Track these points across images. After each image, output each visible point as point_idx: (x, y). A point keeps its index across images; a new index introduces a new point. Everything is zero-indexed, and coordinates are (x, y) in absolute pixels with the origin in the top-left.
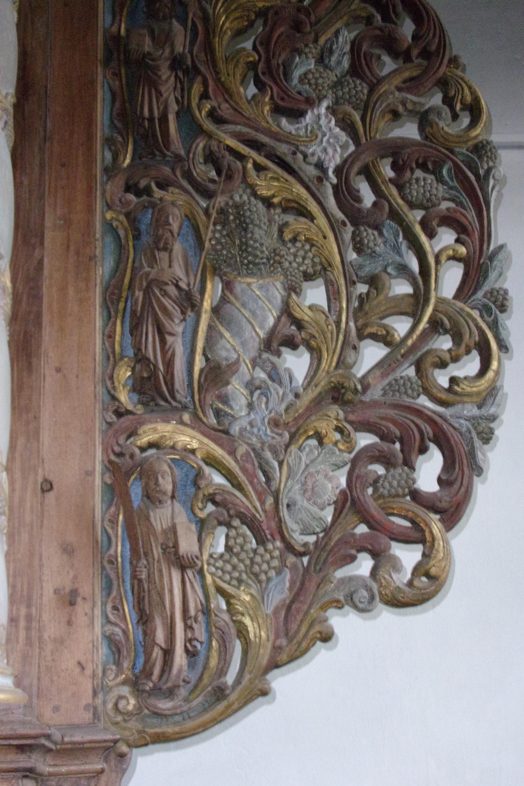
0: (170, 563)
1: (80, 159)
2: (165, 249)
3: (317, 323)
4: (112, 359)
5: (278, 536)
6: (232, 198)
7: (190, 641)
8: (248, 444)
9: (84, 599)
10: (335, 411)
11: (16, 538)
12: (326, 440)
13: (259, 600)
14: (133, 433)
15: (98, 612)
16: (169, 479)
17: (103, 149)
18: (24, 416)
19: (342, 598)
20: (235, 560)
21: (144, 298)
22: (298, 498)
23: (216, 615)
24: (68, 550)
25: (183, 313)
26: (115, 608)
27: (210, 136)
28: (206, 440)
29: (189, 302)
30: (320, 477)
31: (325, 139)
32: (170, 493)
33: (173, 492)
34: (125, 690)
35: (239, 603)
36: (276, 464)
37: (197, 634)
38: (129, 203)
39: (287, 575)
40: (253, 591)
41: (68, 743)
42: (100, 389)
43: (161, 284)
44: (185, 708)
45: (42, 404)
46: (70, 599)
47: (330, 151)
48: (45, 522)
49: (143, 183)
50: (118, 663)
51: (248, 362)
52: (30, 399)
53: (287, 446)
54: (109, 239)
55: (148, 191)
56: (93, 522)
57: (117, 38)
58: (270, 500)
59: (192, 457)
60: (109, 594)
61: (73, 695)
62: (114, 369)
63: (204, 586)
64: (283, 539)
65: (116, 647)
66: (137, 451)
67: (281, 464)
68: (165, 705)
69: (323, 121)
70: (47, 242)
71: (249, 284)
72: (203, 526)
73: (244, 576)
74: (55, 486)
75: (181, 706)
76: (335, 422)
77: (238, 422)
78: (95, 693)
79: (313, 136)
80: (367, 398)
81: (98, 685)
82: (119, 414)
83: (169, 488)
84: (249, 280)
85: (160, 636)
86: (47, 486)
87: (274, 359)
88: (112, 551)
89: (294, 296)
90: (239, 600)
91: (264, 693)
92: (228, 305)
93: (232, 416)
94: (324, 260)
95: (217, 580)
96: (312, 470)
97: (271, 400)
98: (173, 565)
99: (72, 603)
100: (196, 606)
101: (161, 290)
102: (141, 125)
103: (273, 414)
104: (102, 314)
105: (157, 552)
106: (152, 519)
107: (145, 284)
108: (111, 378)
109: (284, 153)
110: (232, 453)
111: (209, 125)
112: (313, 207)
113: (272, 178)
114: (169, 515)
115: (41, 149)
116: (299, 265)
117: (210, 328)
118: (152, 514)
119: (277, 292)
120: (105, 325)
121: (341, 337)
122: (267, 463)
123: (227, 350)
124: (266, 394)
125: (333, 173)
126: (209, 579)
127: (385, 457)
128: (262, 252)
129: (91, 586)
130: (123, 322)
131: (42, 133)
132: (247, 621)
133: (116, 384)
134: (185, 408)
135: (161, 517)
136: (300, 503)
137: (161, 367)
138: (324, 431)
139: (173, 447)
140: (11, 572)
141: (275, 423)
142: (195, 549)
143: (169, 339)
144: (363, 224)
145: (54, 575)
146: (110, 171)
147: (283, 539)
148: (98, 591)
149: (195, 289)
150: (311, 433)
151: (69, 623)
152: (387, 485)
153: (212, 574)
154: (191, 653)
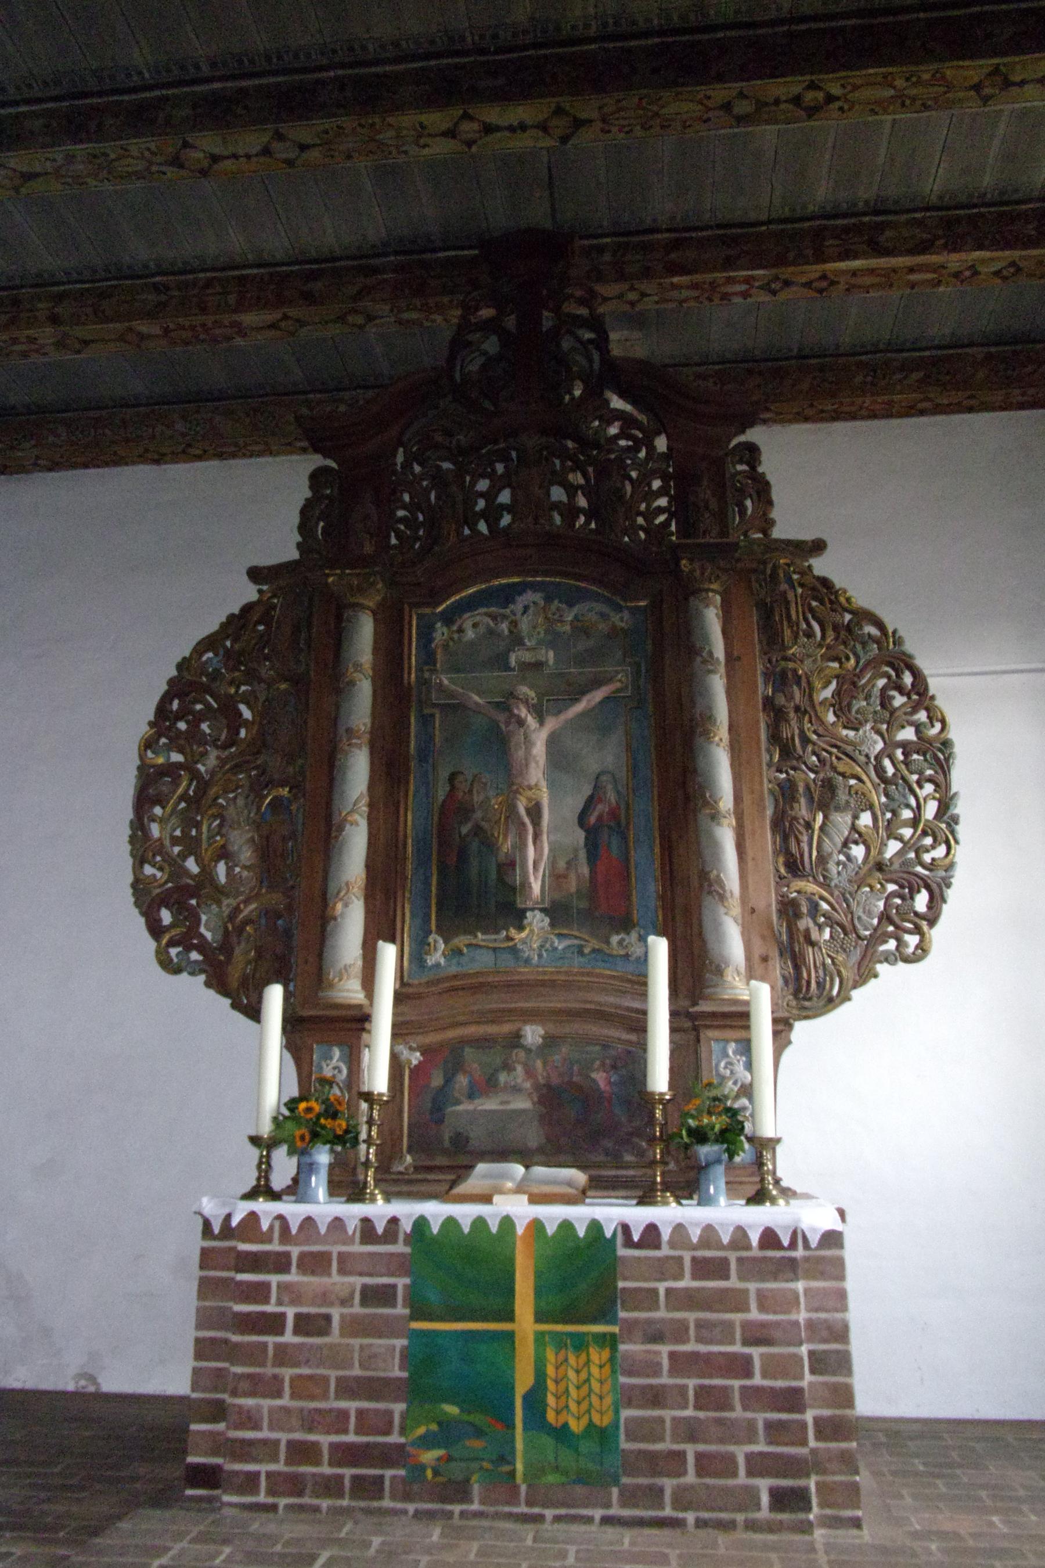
29: (809, 826)
46: (765, 959)
111: (814, 737)
119: (849, 819)
129: (774, 953)
145: (759, 950)
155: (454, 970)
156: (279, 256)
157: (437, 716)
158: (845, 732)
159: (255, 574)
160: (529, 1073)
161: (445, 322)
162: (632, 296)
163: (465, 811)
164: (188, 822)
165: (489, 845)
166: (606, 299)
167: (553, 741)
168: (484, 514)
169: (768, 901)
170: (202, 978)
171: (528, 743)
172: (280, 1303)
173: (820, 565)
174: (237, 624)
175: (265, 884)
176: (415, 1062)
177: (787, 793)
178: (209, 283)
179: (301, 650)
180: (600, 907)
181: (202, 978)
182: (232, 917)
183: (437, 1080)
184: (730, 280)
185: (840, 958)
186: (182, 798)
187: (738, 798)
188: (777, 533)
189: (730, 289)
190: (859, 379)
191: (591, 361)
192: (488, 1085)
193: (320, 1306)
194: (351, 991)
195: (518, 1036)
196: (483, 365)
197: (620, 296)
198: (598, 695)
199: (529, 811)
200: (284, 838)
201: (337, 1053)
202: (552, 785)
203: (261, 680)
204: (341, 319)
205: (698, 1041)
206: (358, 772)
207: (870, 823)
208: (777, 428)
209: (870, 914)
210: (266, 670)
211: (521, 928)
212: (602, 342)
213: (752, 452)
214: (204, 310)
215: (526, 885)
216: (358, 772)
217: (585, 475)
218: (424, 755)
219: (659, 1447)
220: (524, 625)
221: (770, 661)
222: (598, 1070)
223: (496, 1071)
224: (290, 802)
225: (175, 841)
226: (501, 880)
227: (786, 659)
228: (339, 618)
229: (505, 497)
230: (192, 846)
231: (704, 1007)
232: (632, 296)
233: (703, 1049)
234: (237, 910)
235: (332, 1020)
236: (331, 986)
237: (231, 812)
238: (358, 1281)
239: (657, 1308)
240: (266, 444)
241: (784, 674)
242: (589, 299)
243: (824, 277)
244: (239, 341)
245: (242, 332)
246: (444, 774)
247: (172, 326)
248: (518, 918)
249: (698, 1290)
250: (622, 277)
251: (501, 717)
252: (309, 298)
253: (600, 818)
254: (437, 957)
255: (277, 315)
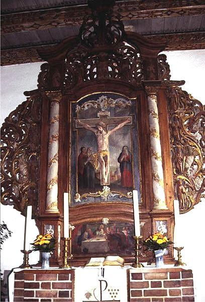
4: (173, 168)
24: (170, 192)
29: (182, 160)
46: (171, 198)
57: (170, 124)
61: (134, 8)
72: (186, 188)
82: (175, 175)
86: (167, 184)
111: (183, 135)
119: (193, 158)
124: (192, 171)
129: (173, 196)
135: (180, 188)
140: (150, 161)
145: (169, 195)
155: (83, 203)
156: (34, 8)
157: (77, 132)
158: (191, 134)
159: (26, 93)
160: (105, 231)
161: (78, 24)
162: (130, 16)
163: (86, 158)
164: (8, 162)
165: (92, 168)
166: (123, 17)
167: (110, 138)
168: (89, 75)
169: (171, 181)
170: (13, 206)
171: (103, 138)
172: (36, 297)
173: (184, 88)
174: (21, 107)
175: (30, 180)
176: (73, 229)
177: (176, 151)
178: (15, 15)
179: (39, 114)
180: (122, 185)
181: (13, 206)
182: (21, 190)
183: (79, 234)
184: (157, 11)
185: (191, 197)
186: (7, 156)
187: (162, 153)
188: (171, 79)
189: (156, 14)
190: (192, 38)
191: (120, 33)
192: (94, 235)
193: (48, 297)
194: (54, 209)
195: (101, 221)
196: (89, 35)
197: (127, 16)
198: (123, 124)
199: (103, 158)
200: (35, 167)
201: (51, 227)
202: (110, 150)
203: (28, 123)
204: (50, 24)
205: (152, 221)
206: (55, 147)
207: (198, 159)
208: (170, 52)
209: (199, 184)
210: (30, 121)
211: (102, 191)
212: (122, 28)
213: (164, 57)
214: (13, 23)
215: (103, 178)
216: (55, 147)
217: (117, 64)
218: (74, 142)
219: (141, 297)
220: (102, 105)
221: (170, 114)
222: (124, 230)
223: (96, 231)
224: (37, 157)
225: (5, 168)
226: (96, 177)
227: (175, 113)
228: (50, 104)
229: (95, 70)
230: (10, 169)
231: (154, 211)
232: (130, 16)
233: (154, 223)
234: (23, 187)
235: (51, 217)
236: (49, 208)
237: (20, 160)
238: (58, 290)
239: (142, 296)
240: (31, 59)
241: (174, 117)
242: (119, 17)
243: (182, 11)
244: (23, 31)
245: (23, 28)
246: (79, 148)
247: (5, 28)
248: (101, 188)
249: (152, 290)
250: (127, 10)
251: (95, 131)
252: (42, 19)
253: (124, 159)
254: (78, 200)
255: (33, 24)
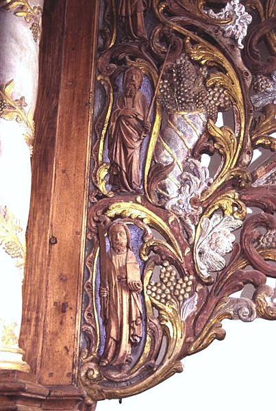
0: (122, 287)
1: (84, 46)
2: (130, 96)
3: (225, 138)
5: (192, 272)
6: (175, 62)
7: (133, 336)
8: (177, 215)
9: (71, 308)
10: (233, 194)
11: (33, 271)
12: (226, 212)
13: (178, 312)
14: (106, 209)
15: (79, 317)
16: (125, 236)
17: (98, 36)
18: (42, 200)
19: (232, 313)
20: (164, 287)
21: (116, 127)
22: (206, 248)
23: (150, 321)
25: (140, 135)
26: (89, 314)
27: (164, 24)
28: (150, 212)
29: (144, 129)
30: (221, 235)
31: (237, 21)
32: (125, 244)
33: (128, 244)
34: (92, 365)
35: (164, 313)
36: (193, 227)
37: (137, 333)
38: (111, 69)
39: (196, 297)
40: (174, 306)
41: (53, 396)
42: (87, 182)
43: (126, 118)
44: (128, 378)
45: (52, 192)
46: (62, 308)
47: (240, 28)
48: (51, 262)
49: (121, 56)
50: (89, 349)
51: (180, 164)
52: (46, 189)
53: (201, 215)
54: (98, 92)
55: (124, 61)
56: (79, 262)
58: (188, 250)
59: (141, 223)
60: (87, 306)
62: (97, 169)
63: (144, 303)
64: (195, 274)
65: (89, 339)
66: (108, 219)
67: (196, 227)
68: (115, 375)
69: (237, 10)
70: (60, 96)
71: (183, 116)
72: (144, 266)
73: (169, 297)
74: (58, 241)
75: (125, 377)
76: (233, 201)
77: (171, 201)
78: (74, 367)
79: (231, 18)
80: (255, 185)
81: (76, 361)
82: (100, 196)
83: (124, 241)
84: (183, 113)
85: (113, 332)
86: (53, 241)
87: (197, 162)
88: (89, 281)
89: (211, 121)
90: (165, 312)
91: (179, 371)
92: (170, 129)
93: (168, 198)
94: (231, 99)
95: (152, 299)
96: (216, 230)
97: (192, 187)
98: (125, 290)
99: (64, 311)
100: (137, 314)
101: (126, 121)
102: (121, 21)
103: (193, 196)
104: (91, 137)
105: (115, 281)
106: (114, 261)
107: (116, 118)
108: (95, 176)
109: (210, 32)
110: (166, 221)
112: (227, 65)
113: (200, 48)
114: (124, 258)
115: (60, 40)
116: (216, 102)
117: (158, 144)
118: (114, 257)
119: (201, 117)
120: (93, 145)
121: (240, 146)
122: (188, 226)
123: (167, 157)
125: (242, 43)
126: (147, 298)
127: (265, 222)
128: (190, 95)
130: (104, 142)
131: (61, 31)
132: (169, 324)
133: (98, 179)
134: (138, 193)
136: (207, 251)
137: (124, 169)
138: (225, 207)
139: (130, 217)
141: (194, 202)
142: (138, 279)
143: (130, 151)
144: (260, 74)
145: (54, 295)
146: (100, 50)
147: (195, 274)
148: (79, 303)
149: (148, 120)
150: (217, 207)
151: (61, 323)
152: (265, 241)
153: (150, 295)
154: (133, 344)
